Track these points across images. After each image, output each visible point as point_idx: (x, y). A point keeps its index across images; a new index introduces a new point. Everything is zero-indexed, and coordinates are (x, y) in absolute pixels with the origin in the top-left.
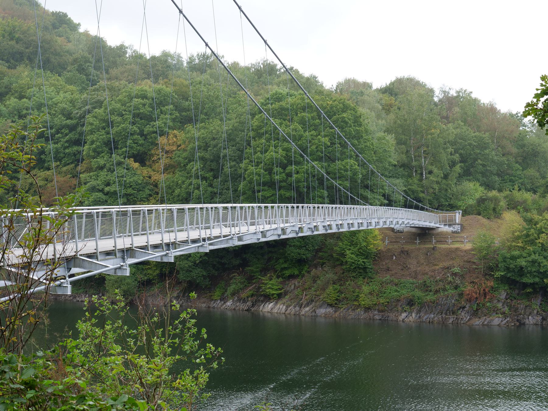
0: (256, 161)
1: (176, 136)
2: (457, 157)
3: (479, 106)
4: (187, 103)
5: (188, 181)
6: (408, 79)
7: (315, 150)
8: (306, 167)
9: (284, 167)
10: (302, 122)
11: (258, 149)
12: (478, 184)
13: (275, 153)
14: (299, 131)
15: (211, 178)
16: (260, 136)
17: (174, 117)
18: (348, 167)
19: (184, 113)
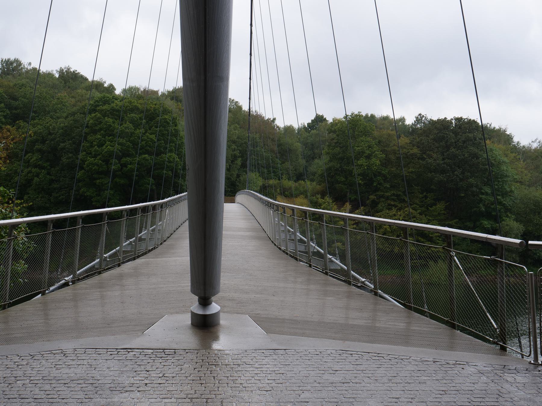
1: (9, 131)
2: (237, 153)
3: (158, 98)
7: (145, 145)
8: (138, 159)
9: (119, 158)
10: (132, 121)
11: (95, 143)
14: (131, 129)
15: (49, 167)
16: (95, 132)
17: (5, 114)
19: (14, 111)
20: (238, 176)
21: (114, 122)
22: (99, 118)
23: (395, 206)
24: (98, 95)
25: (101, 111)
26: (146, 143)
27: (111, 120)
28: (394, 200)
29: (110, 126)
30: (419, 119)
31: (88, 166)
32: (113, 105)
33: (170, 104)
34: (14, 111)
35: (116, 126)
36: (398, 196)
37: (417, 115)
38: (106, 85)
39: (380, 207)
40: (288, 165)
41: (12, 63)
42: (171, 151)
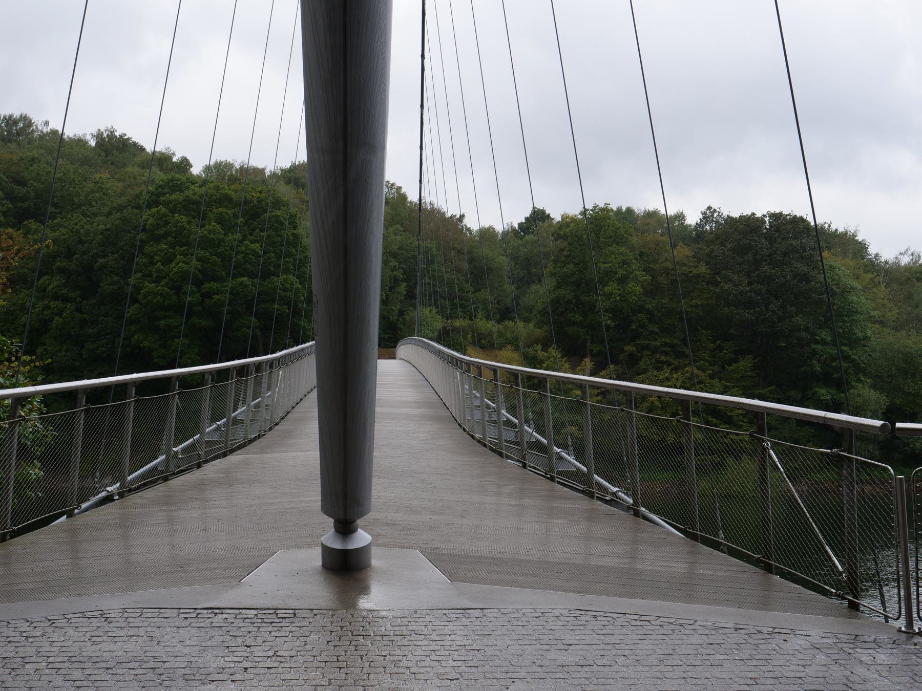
0: (155, 275)
1: (11, 237)
2: (399, 274)
4: (24, 190)
5: (41, 304)
6: (226, 164)
9: (198, 283)
10: (220, 220)
12: (435, 310)
13: (186, 264)
15: (78, 299)
16: (158, 239)
17: (5, 209)
18: (288, 286)
19: (20, 204)
20: (401, 313)
21: (189, 223)
22: (164, 215)
23: (669, 364)
24: (159, 176)
25: (167, 204)
26: (244, 257)
27: (184, 219)
28: (666, 354)
29: (183, 228)
30: (709, 215)
31: (145, 297)
32: (189, 193)
33: (285, 191)
34: (20, 204)
35: (194, 228)
36: (672, 346)
37: (704, 208)
38: (174, 159)
39: (642, 364)
40: (484, 294)
41: (16, 122)
42: (287, 271)
